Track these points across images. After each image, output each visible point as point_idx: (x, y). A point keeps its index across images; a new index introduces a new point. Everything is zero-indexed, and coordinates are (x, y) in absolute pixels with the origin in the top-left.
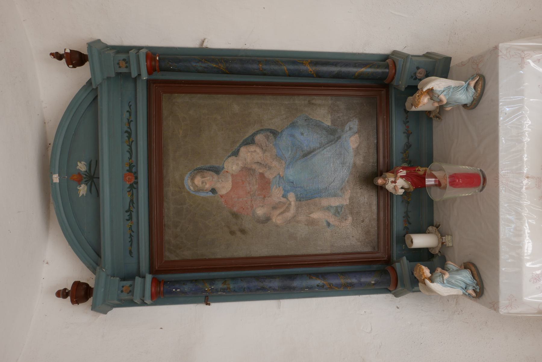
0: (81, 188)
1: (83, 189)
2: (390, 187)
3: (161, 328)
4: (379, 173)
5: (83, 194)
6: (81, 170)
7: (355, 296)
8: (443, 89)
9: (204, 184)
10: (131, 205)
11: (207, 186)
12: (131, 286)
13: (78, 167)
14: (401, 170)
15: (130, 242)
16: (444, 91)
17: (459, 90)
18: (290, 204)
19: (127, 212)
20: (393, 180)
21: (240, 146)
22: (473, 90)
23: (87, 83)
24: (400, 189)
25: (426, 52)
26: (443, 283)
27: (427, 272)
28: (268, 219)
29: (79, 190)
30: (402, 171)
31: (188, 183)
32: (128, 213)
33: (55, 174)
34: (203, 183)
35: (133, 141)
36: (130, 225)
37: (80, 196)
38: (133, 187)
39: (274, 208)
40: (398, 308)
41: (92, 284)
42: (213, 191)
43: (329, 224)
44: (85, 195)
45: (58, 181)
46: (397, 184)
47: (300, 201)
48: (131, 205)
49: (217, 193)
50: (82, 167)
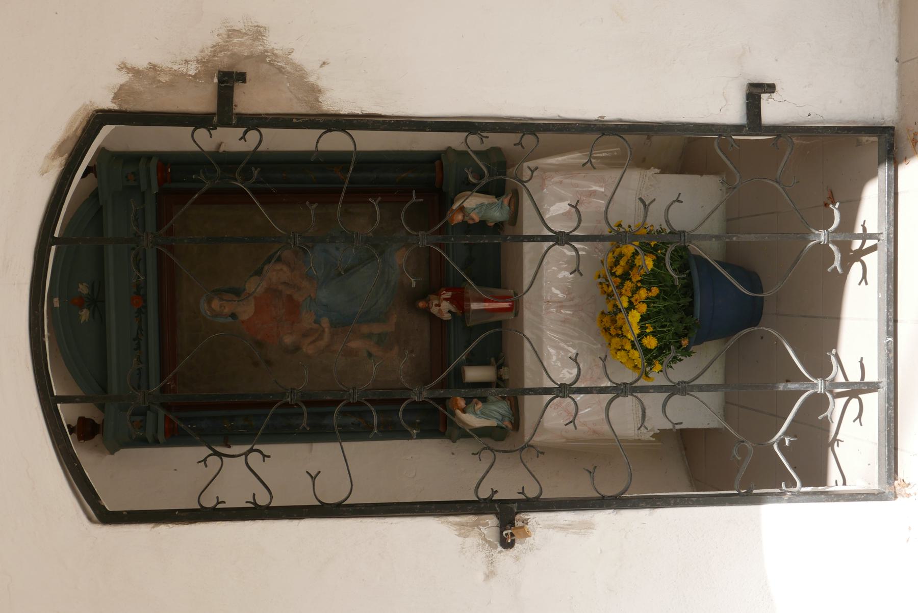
0: (83, 313)
1: (85, 315)
2: (434, 310)
3: (176, 470)
4: (424, 296)
5: (85, 320)
6: (82, 292)
7: (402, 441)
8: (474, 207)
9: (223, 308)
10: (139, 332)
11: (227, 311)
12: (141, 421)
13: (79, 290)
14: (444, 292)
15: (138, 374)
16: (475, 209)
17: (492, 207)
18: (323, 331)
19: (134, 340)
20: (437, 303)
21: (264, 264)
22: (508, 208)
23: (90, 196)
24: (446, 313)
25: (490, 146)
26: (475, 413)
27: (462, 403)
28: (297, 348)
29: (80, 315)
30: (445, 293)
31: (204, 306)
32: (137, 342)
33: (56, 297)
34: (221, 307)
35: (140, 260)
36: (138, 356)
37: (82, 322)
38: (142, 311)
39: (305, 335)
40: (453, 454)
41: (97, 421)
42: (233, 316)
43: (370, 355)
44: (87, 320)
45: (58, 306)
46: (441, 307)
47: (335, 327)
48: (139, 332)
49: (877, 244)
50: (84, 289)
